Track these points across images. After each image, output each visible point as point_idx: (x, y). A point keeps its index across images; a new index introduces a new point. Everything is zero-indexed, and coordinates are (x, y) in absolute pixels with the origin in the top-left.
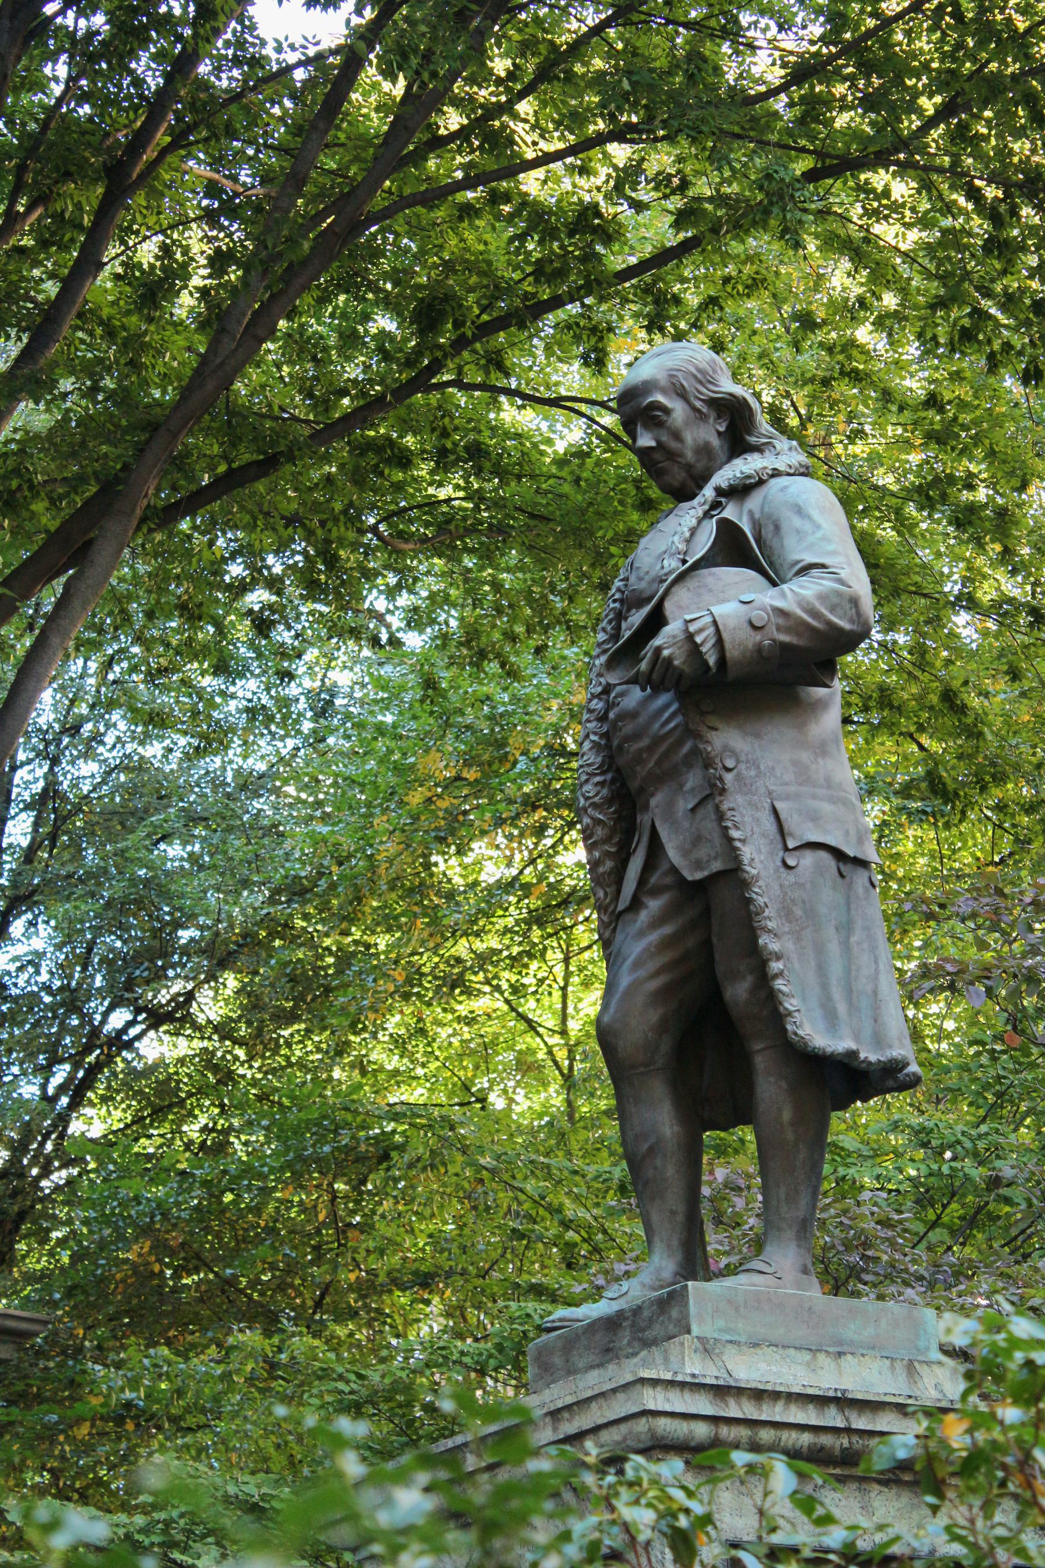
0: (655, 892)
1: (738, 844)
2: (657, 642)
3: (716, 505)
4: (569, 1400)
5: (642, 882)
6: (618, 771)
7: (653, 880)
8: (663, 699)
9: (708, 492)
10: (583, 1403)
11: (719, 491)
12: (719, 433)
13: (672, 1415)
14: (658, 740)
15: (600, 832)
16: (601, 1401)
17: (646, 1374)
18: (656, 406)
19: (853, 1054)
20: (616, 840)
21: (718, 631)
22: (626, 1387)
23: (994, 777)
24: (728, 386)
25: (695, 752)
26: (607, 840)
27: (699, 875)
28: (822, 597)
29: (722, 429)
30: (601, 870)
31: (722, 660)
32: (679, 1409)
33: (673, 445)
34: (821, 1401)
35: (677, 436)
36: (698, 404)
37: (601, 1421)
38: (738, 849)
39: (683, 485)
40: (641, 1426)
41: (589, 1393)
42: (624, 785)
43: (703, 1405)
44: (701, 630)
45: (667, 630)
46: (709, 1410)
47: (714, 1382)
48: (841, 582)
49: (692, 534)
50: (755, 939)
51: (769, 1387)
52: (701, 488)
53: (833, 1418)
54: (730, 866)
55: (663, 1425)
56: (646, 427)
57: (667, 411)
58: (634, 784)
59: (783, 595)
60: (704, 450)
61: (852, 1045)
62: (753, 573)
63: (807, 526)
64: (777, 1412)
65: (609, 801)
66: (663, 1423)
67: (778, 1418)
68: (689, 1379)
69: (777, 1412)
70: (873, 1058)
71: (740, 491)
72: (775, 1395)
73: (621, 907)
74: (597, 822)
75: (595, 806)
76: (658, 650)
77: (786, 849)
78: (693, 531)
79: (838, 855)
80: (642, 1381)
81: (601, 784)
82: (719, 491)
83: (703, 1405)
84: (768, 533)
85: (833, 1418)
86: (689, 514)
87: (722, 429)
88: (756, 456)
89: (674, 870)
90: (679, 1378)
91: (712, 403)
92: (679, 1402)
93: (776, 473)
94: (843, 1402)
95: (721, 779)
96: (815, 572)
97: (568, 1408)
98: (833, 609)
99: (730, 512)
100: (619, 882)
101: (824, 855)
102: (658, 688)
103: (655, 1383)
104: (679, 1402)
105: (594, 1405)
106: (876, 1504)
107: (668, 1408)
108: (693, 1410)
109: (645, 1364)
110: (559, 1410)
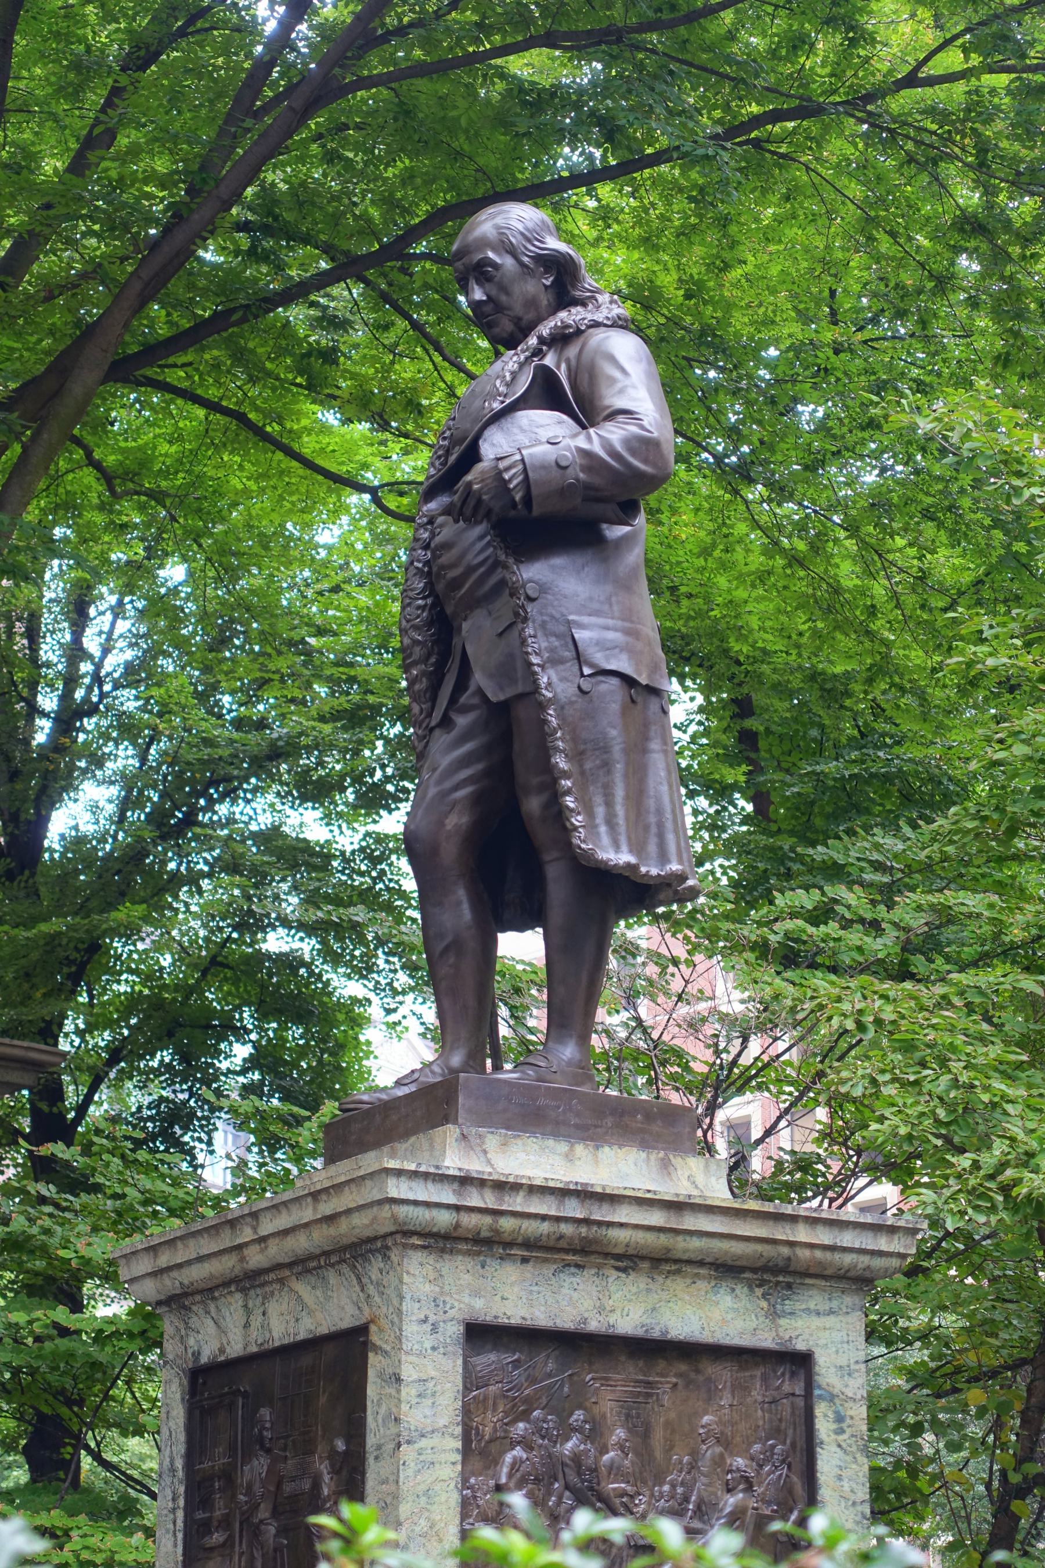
0: (465, 710)
1: (537, 669)
2: (469, 477)
3: (538, 353)
4: (327, 1184)
5: (453, 700)
6: (437, 597)
7: (463, 700)
8: (478, 530)
9: (533, 341)
10: (338, 1188)
11: (541, 340)
12: (546, 287)
13: (416, 1203)
14: (471, 570)
15: (417, 652)
16: (353, 1186)
17: (392, 1164)
18: (487, 262)
19: (633, 868)
20: (433, 660)
21: (525, 470)
22: (372, 1175)
23: (223, 550)
24: (554, 243)
25: (503, 583)
26: (425, 659)
27: (502, 697)
28: (627, 442)
29: (548, 283)
30: (417, 687)
31: (528, 499)
32: (421, 1198)
33: (503, 298)
34: (563, 1193)
35: (504, 289)
36: (526, 259)
37: (352, 1205)
38: (535, 673)
39: (512, 335)
40: (386, 1212)
41: (343, 1179)
42: (442, 610)
43: (446, 1195)
44: (508, 469)
45: (479, 467)
46: (449, 1198)
47: (457, 1173)
48: (642, 428)
49: (513, 379)
50: (548, 758)
51: (511, 1179)
52: (526, 336)
53: (574, 1209)
54: (528, 689)
55: (403, 1211)
56: (479, 283)
57: (496, 266)
58: (449, 610)
59: (589, 438)
60: (531, 303)
61: (633, 860)
62: (565, 417)
63: (617, 374)
64: (517, 1203)
65: (430, 623)
66: (403, 1211)
67: (519, 1209)
68: (432, 1170)
69: (517, 1203)
70: (654, 872)
71: (562, 339)
72: (515, 1187)
73: (433, 723)
74: (415, 642)
75: (415, 628)
76: (469, 484)
77: (582, 675)
78: (514, 375)
79: (629, 681)
80: (387, 1171)
81: (423, 608)
82: (541, 340)
83: (446, 1195)
84: (584, 380)
85: (574, 1209)
86: (511, 360)
87: (548, 283)
88: (579, 308)
89: (480, 692)
90: (423, 1169)
91: (538, 259)
92: (421, 1192)
93: (596, 324)
94: (584, 1194)
95: (523, 607)
96: (621, 418)
97: (325, 1190)
98: (633, 452)
99: (549, 361)
100: (434, 700)
101: (615, 681)
102: (472, 520)
103: (399, 1173)
104: (421, 1192)
105: (368, 1183)
106: (613, 1288)
107: (411, 1196)
108: (435, 1199)
109: (393, 1156)
110: (319, 1192)
